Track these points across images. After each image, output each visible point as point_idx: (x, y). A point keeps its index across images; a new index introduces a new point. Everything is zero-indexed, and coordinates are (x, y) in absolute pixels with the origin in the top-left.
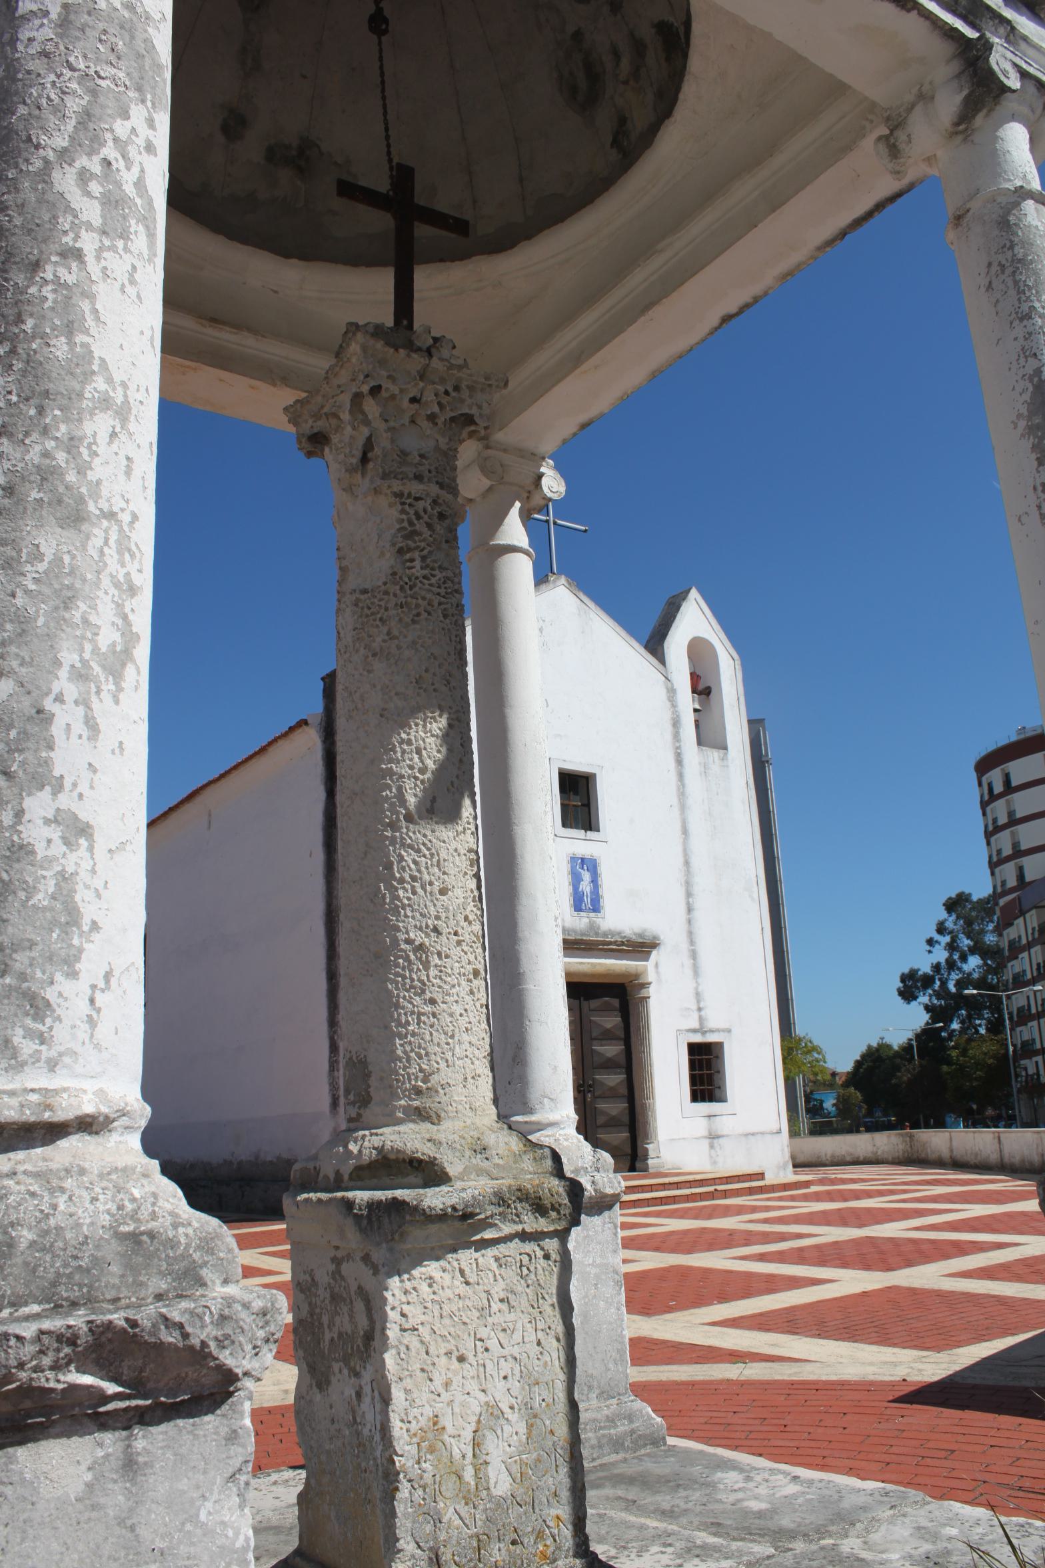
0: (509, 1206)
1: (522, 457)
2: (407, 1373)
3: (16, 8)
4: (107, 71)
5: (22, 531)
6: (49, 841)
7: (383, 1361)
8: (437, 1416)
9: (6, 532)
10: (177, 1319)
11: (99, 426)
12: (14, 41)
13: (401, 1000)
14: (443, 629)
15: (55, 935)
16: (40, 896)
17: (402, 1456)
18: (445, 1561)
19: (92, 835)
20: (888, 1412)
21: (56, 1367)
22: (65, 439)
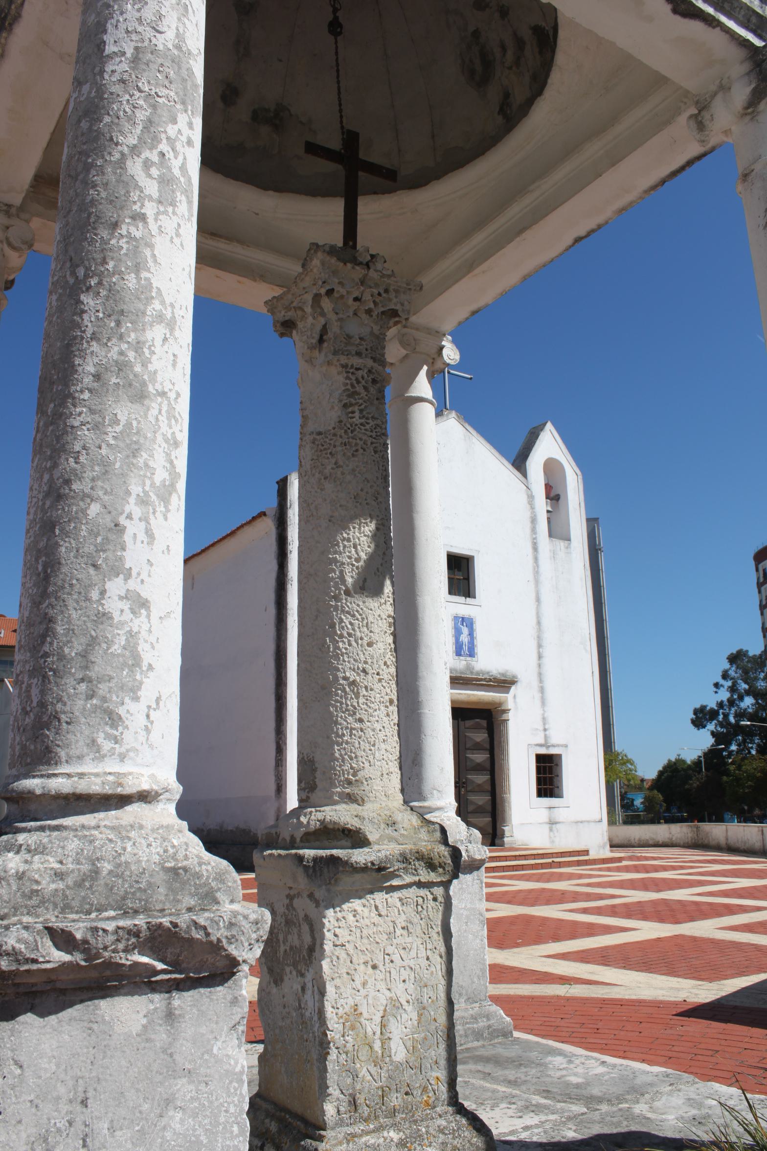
0: (410, 863)
1: (430, 334)
2: (337, 975)
3: (104, 50)
4: (163, 92)
5: (105, 404)
6: (122, 611)
7: (321, 966)
8: (356, 1005)
9: (95, 404)
10: (203, 924)
11: (156, 333)
12: (102, 72)
13: (339, 719)
14: (374, 461)
15: (125, 673)
16: (116, 647)
17: (332, 1031)
18: (360, 1103)
19: (149, 607)
20: (672, 1022)
21: (126, 950)
22: (134, 343)
